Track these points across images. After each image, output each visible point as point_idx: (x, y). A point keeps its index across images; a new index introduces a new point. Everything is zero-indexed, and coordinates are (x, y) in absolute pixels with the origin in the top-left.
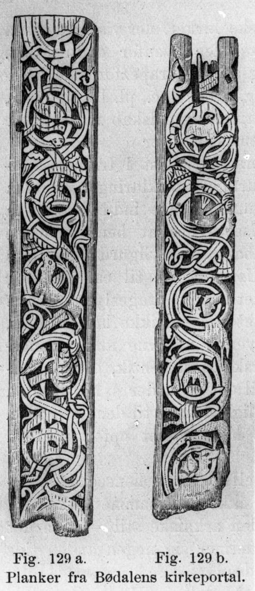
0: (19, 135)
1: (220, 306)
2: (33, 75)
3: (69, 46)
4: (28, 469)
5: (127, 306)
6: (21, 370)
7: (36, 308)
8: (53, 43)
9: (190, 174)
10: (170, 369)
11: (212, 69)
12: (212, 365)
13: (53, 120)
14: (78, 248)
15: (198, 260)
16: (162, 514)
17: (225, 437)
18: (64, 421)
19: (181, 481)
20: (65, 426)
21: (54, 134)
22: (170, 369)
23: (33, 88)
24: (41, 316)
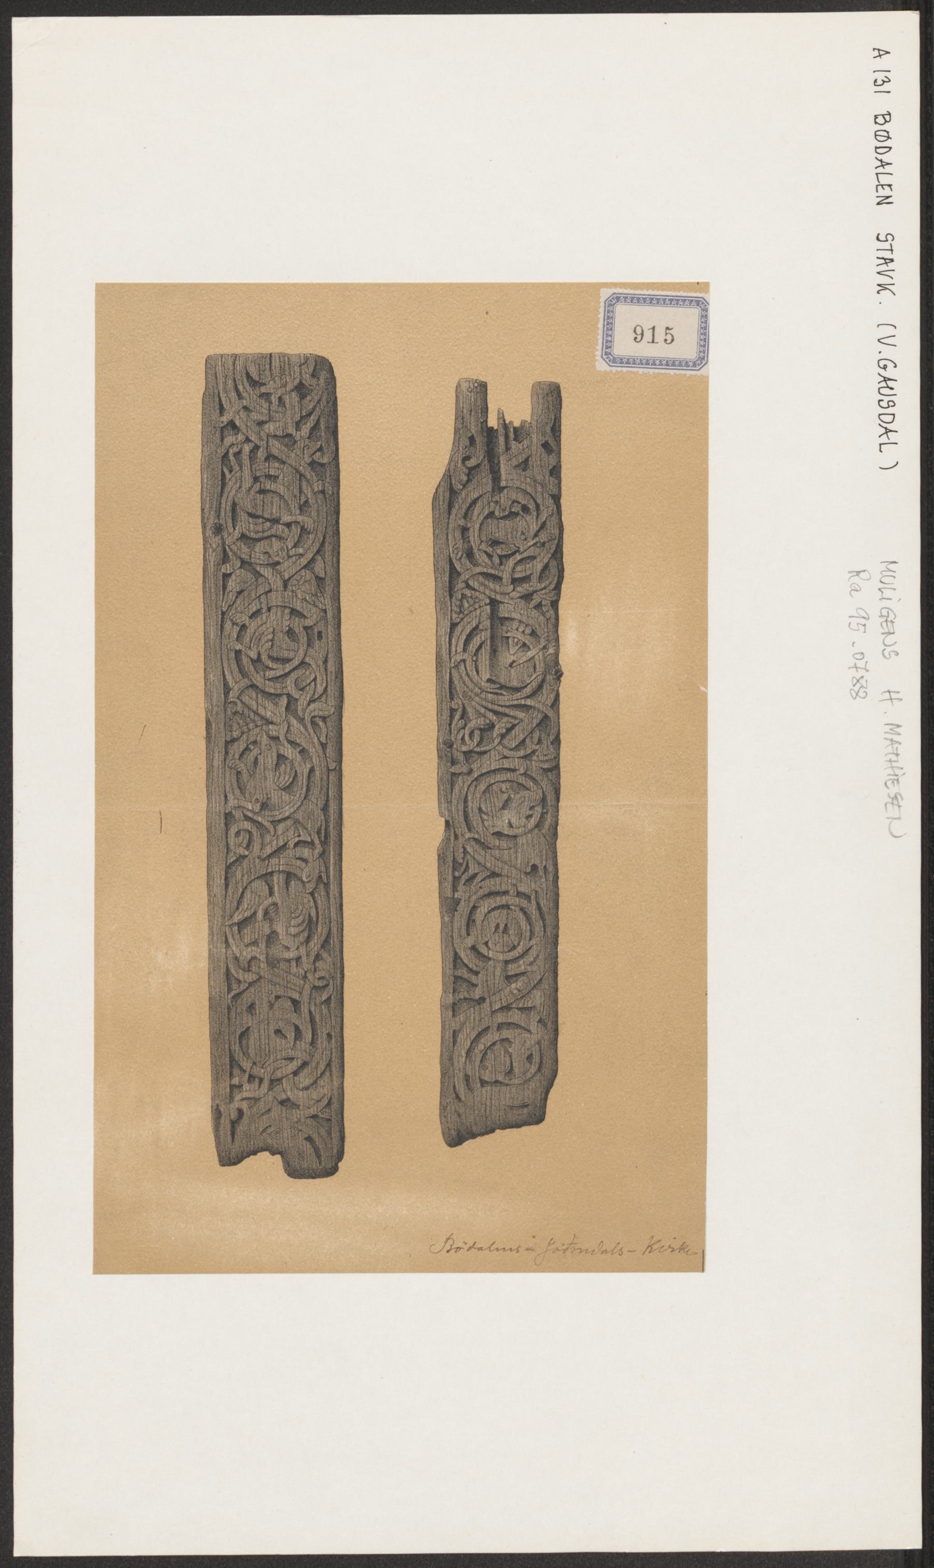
0: (215, 541)
1: (539, 809)
2: (235, 449)
3: (292, 399)
4: (313, 719)
5: (510, 1093)
6: (313, 683)
7: (247, 818)
8: (266, 396)
9: (488, 601)
10: (464, 909)
11: (519, 433)
12: (530, 902)
13: (269, 520)
14: (313, 723)
15: (503, 736)
16: (456, 1139)
17: (517, 954)
18: (296, 996)
19: (483, 1083)
20: (295, 1003)
21: (550, 1093)
22: (464, 909)
23: (237, 468)
24: (254, 830)
